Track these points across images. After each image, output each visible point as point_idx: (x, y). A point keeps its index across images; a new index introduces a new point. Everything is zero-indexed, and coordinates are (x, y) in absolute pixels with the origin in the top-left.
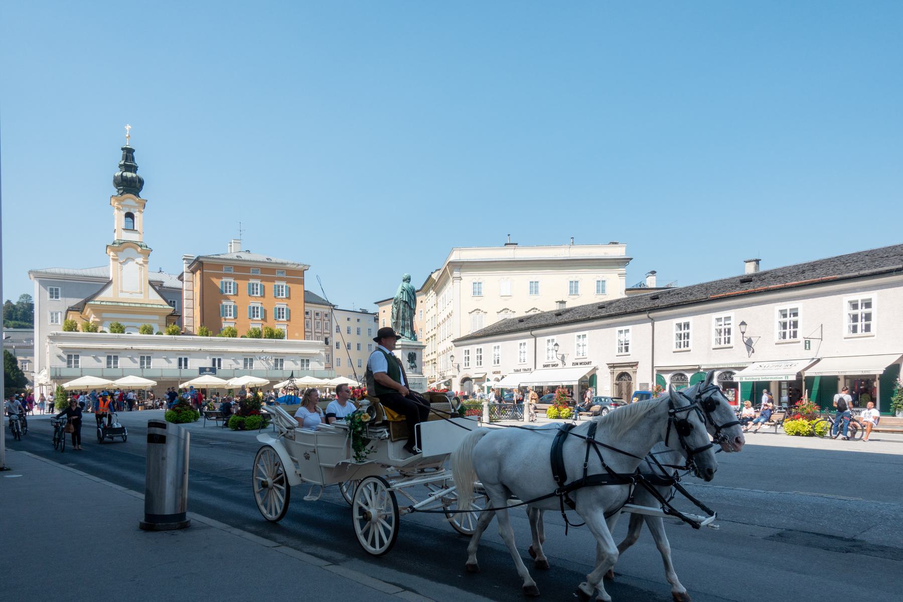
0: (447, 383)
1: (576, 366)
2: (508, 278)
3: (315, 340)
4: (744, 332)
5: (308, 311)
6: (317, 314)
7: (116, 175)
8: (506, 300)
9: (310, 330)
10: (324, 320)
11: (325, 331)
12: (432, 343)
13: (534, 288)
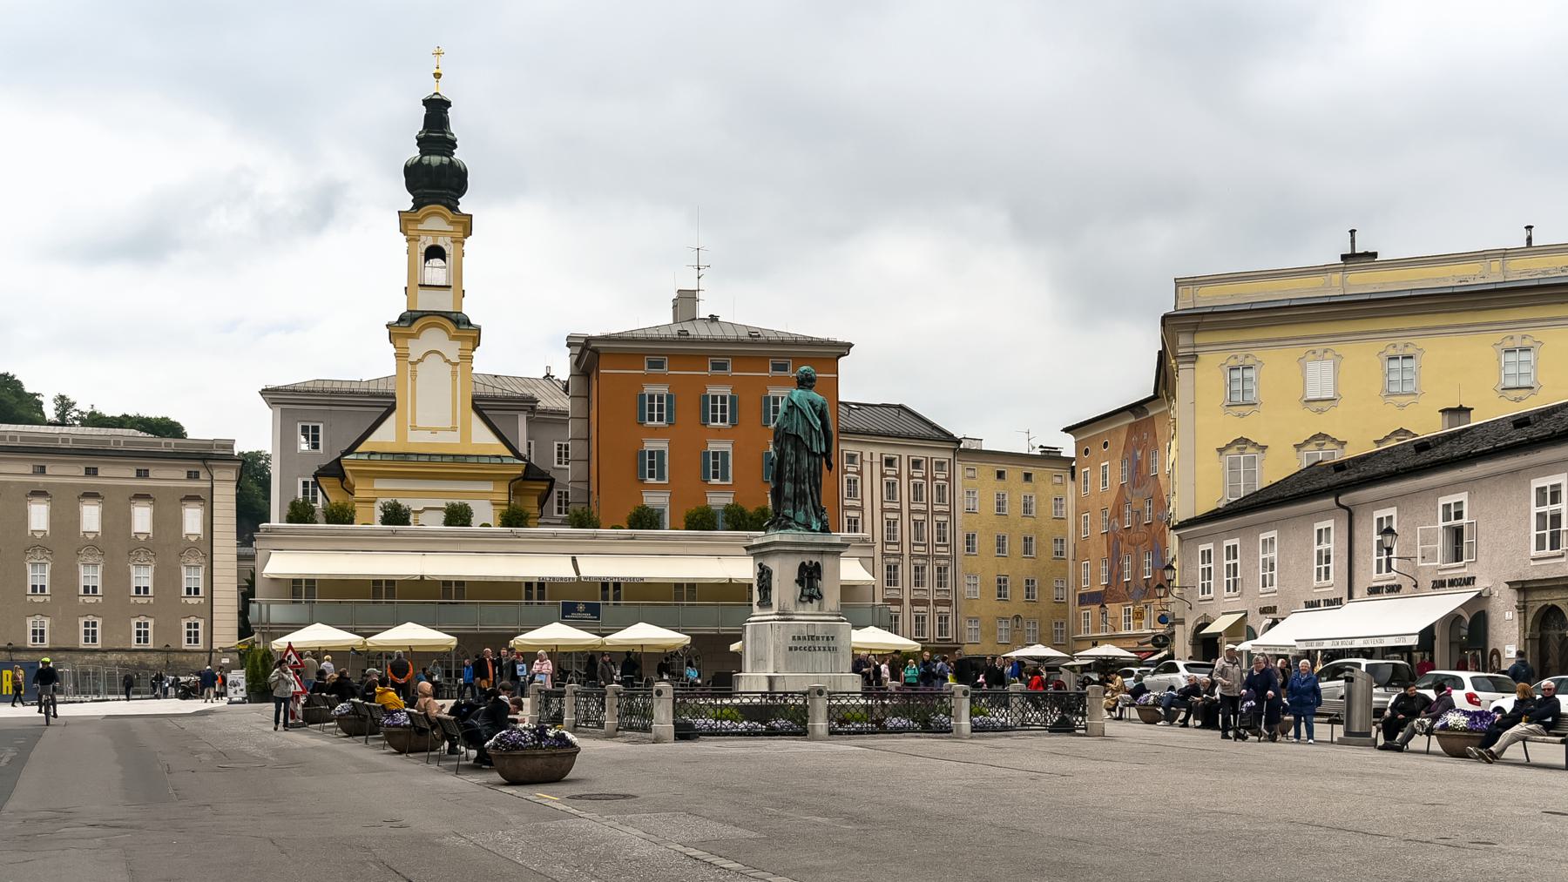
0: (1161, 640)
1: (1441, 591)
2: (1325, 351)
3: (849, 531)
6: (916, 464)
8: (1320, 411)
10: (934, 479)
11: (936, 508)
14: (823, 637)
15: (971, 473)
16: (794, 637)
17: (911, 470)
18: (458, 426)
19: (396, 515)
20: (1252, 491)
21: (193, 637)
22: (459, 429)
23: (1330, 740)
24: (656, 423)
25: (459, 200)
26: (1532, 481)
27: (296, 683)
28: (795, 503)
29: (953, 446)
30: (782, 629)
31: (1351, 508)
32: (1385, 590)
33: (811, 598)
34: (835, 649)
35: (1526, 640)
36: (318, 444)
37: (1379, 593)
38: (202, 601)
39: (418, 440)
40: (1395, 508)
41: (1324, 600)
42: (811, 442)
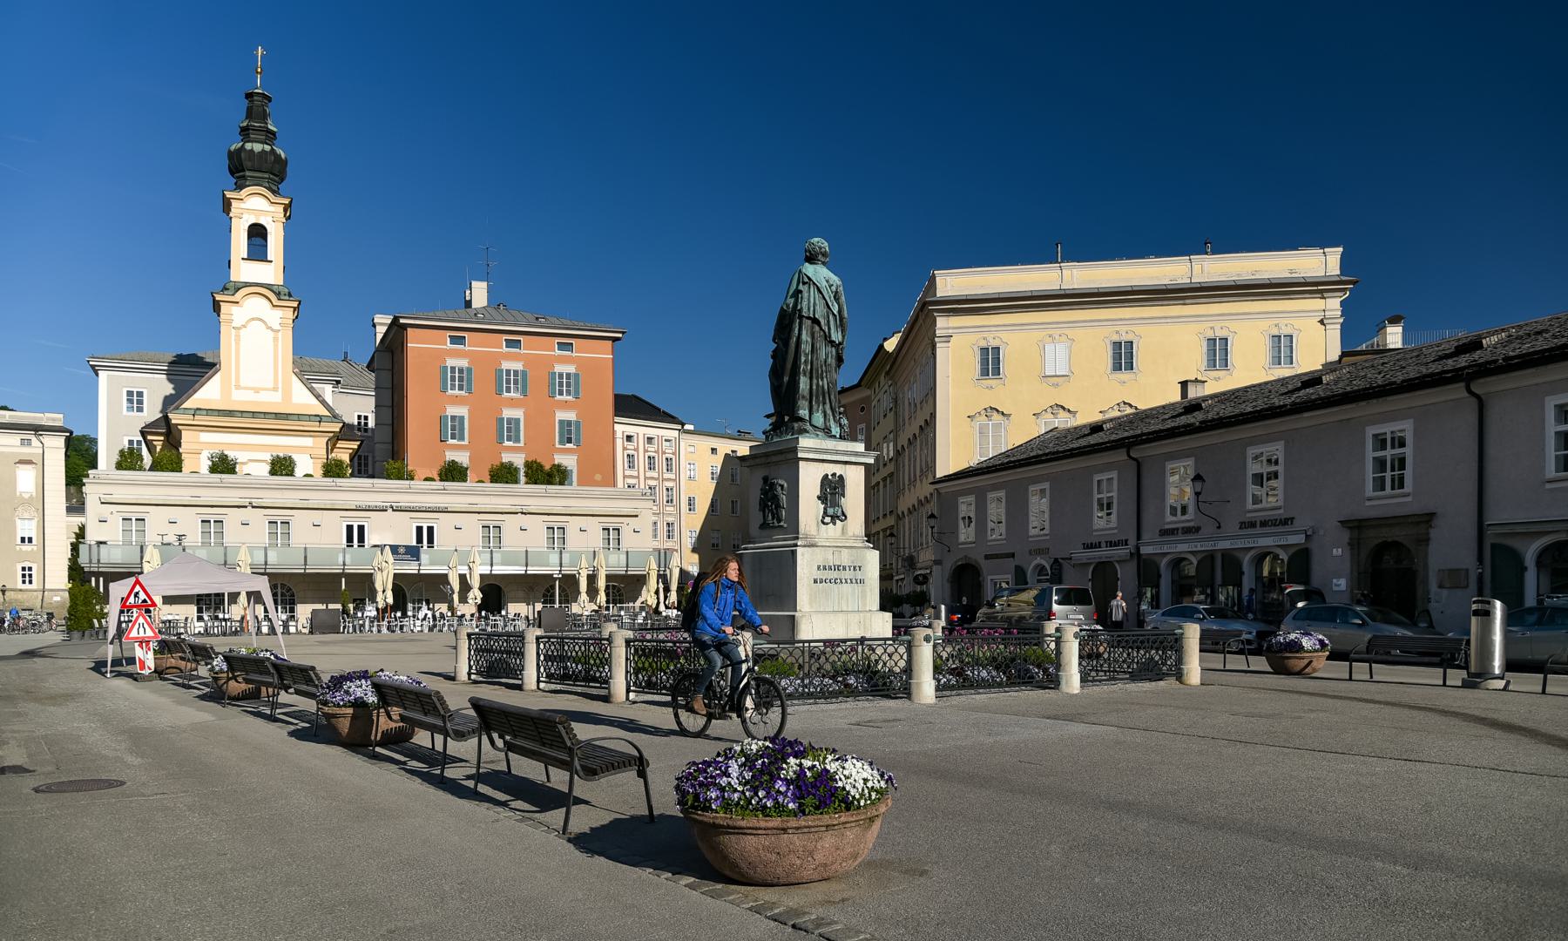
4: (1200, 493)
5: (632, 434)
6: (650, 440)
7: (233, 148)
9: (635, 474)
10: (664, 453)
12: (885, 492)
13: (1123, 357)
14: (850, 567)
15: (692, 449)
16: (819, 568)
17: (646, 446)
18: (280, 385)
19: (223, 465)
20: (1000, 452)
21: (27, 576)
22: (280, 390)
23: (1348, 677)
24: (457, 392)
25: (888, 616)
26: (1367, 428)
27: (146, 625)
28: (811, 402)
29: (680, 427)
30: (806, 556)
31: (1140, 460)
32: (1180, 531)
33: (834, 518)
34: (862, 581)
35: (1359, 574)
36: (142, 408)
37: (1173, 534)
38: (35, 548)
39: (241, 399)
40: (1283, 442)
41: (1106, 542)
42: (829, 329)
